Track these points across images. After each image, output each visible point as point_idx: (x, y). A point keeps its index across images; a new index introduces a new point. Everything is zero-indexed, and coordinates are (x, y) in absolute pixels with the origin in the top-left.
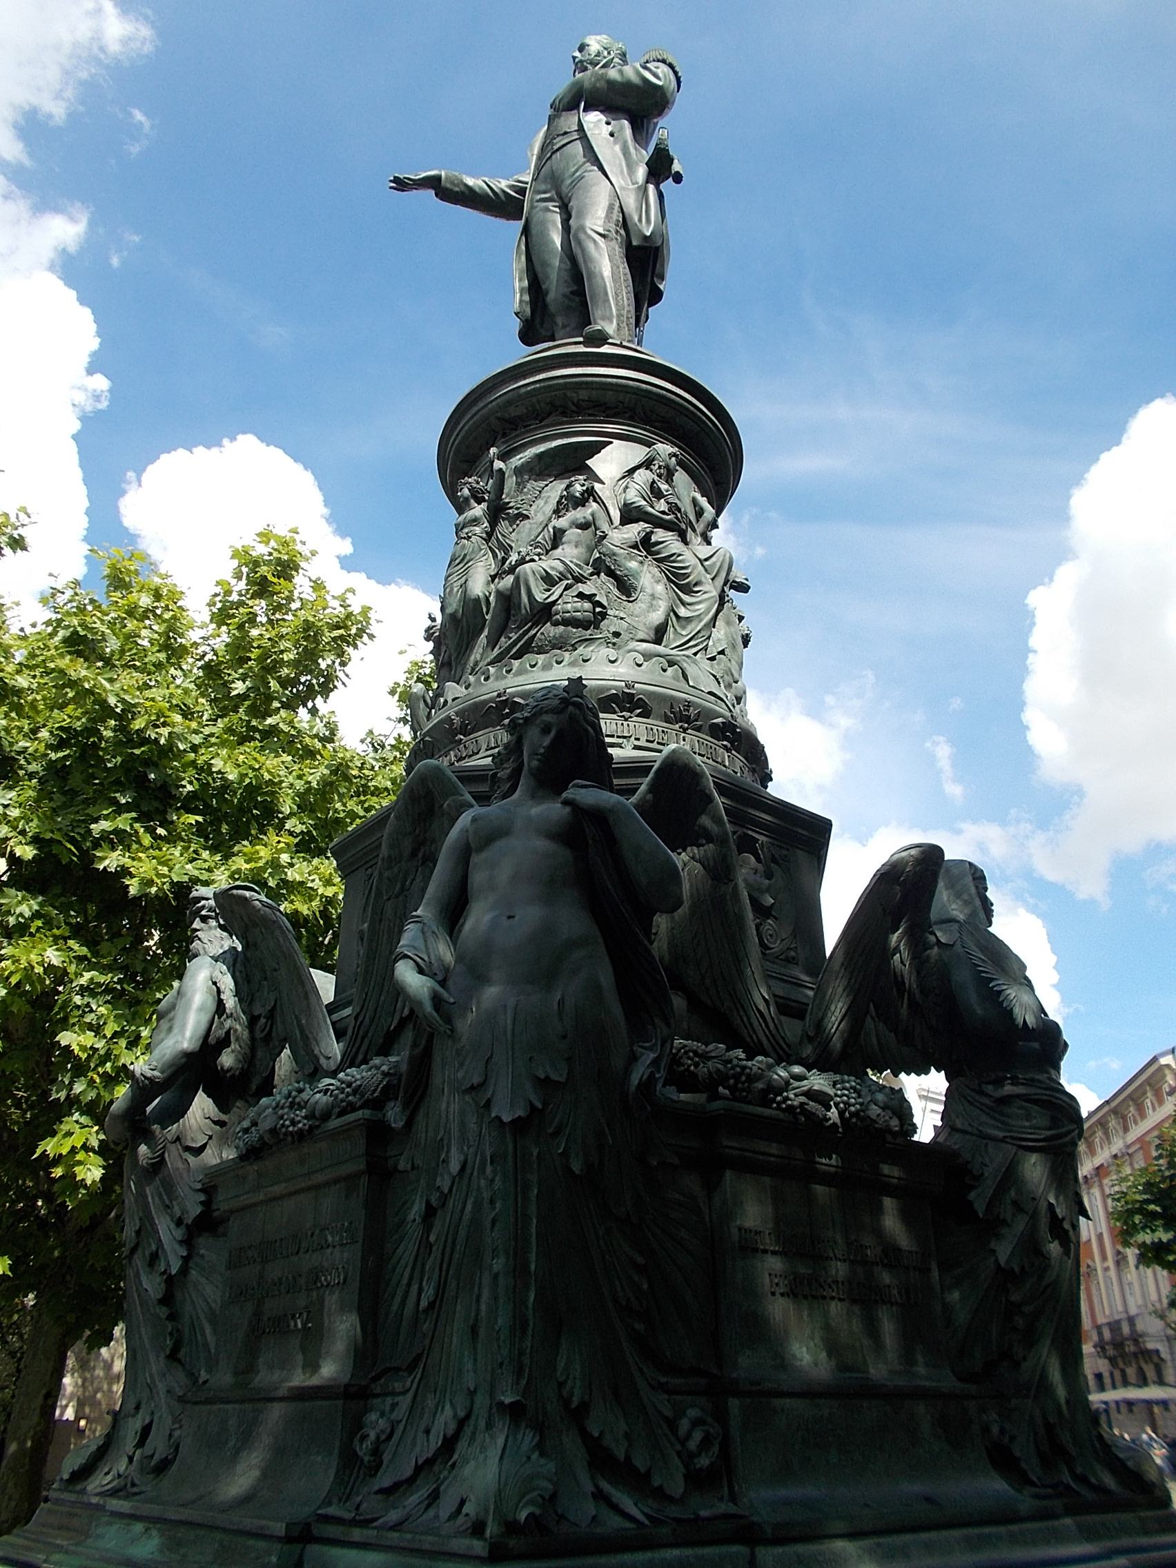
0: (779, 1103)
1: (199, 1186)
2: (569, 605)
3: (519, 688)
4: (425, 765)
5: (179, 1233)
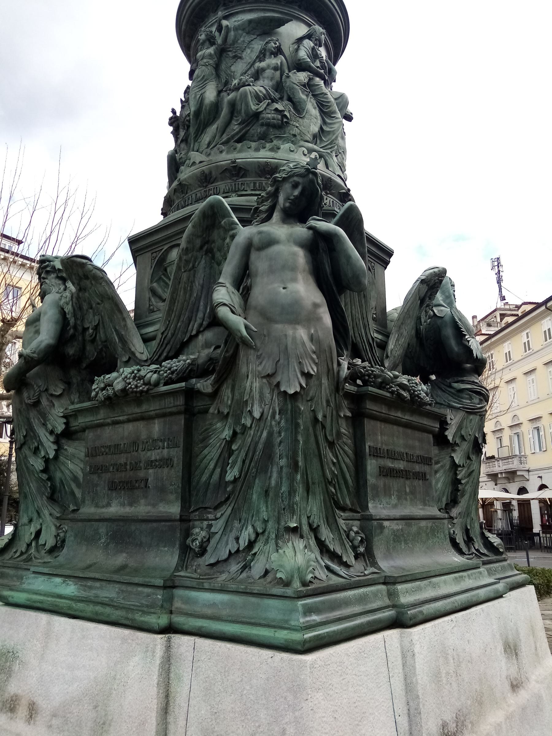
0: (388, 389)
1: (62, 415)
2: (269, 115)
3: (244, 160)
4: (215, 199)
5: (52, 439)
